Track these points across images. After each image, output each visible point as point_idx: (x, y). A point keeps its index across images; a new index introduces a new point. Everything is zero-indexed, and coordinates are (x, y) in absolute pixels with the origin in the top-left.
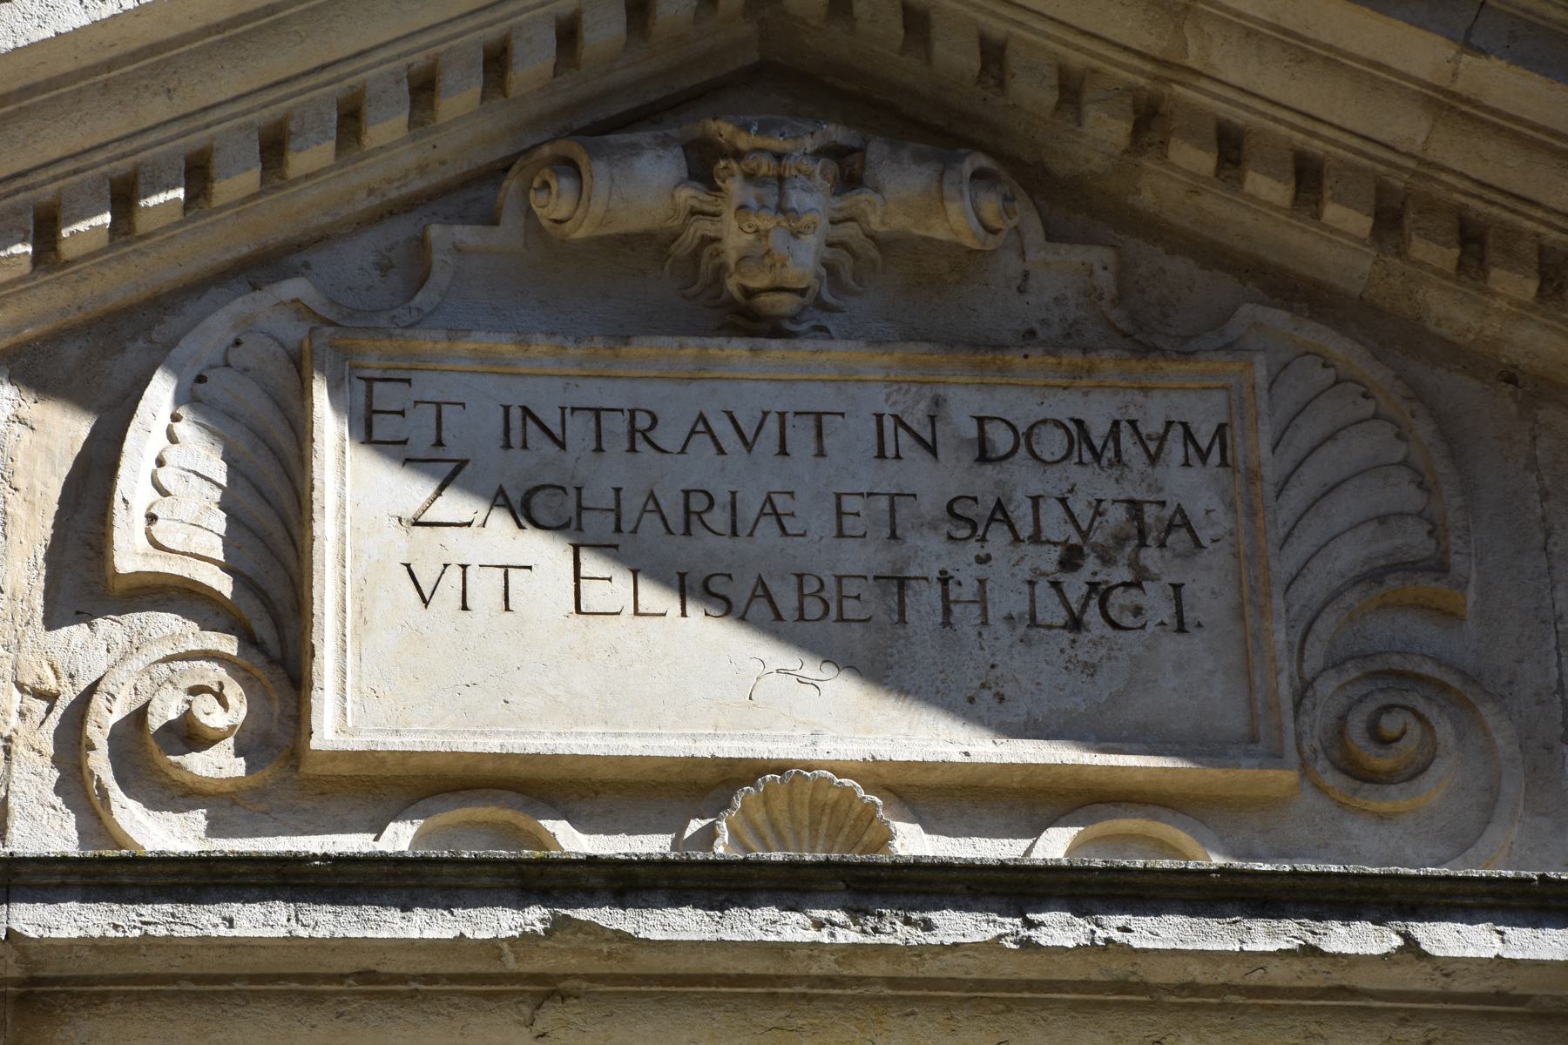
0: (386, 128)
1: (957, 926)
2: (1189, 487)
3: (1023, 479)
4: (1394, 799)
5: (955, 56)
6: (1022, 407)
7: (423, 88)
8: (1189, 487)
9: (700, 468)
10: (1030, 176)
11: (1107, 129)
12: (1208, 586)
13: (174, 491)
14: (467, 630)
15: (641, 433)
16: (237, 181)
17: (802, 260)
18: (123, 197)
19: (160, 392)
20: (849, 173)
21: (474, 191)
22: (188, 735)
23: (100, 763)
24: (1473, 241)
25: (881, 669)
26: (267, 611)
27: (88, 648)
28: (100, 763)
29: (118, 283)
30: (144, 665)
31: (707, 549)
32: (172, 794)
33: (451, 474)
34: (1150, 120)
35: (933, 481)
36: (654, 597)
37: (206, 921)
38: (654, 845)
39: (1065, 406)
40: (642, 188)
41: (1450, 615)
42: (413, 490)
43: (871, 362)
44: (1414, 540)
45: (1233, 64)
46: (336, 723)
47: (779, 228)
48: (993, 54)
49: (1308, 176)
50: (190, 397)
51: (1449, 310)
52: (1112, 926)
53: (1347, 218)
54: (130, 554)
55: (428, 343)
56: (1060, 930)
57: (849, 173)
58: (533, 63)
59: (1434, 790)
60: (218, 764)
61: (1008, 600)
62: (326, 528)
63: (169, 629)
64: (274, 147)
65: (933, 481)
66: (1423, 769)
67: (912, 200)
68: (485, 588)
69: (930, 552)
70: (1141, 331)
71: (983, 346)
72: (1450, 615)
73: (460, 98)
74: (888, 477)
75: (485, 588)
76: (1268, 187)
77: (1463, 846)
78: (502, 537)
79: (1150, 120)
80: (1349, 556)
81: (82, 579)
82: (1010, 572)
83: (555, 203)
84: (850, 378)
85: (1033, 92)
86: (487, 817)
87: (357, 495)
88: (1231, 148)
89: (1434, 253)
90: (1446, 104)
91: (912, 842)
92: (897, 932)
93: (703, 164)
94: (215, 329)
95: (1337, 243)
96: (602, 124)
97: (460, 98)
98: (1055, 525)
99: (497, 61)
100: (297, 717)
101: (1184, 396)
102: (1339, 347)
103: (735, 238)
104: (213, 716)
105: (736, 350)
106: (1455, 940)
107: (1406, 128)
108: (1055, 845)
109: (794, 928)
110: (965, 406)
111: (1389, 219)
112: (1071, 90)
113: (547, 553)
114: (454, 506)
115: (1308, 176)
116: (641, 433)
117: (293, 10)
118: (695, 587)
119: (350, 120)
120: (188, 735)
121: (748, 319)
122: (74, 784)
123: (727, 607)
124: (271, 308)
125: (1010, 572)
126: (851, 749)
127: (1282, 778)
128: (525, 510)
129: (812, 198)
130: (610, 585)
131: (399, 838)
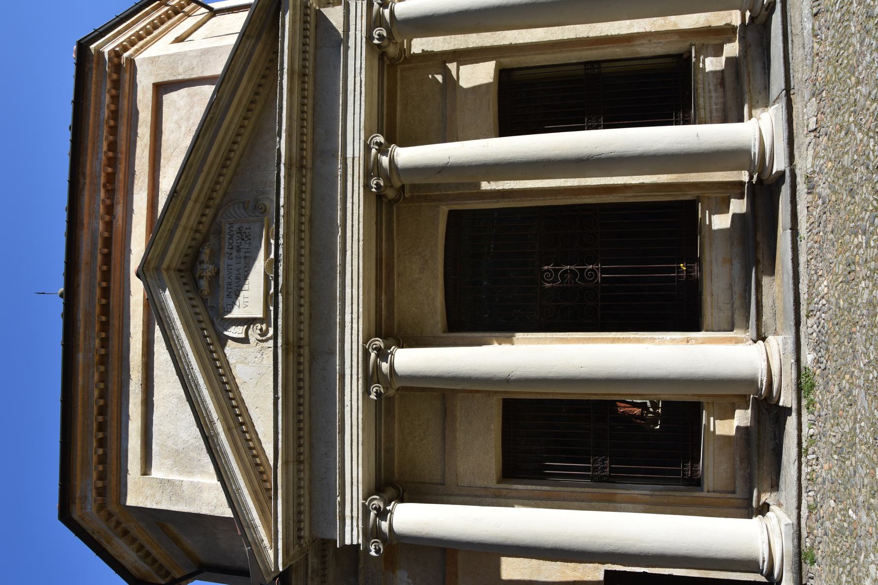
0: (198, 310)
1: (281, 251)
2: (235, 227)
3: (235, 244)
4: (268, 207)
5: (190, 251)
6: (227, 245)
7: (193, 306)
8: (235, 227)
9: (233, 278)
10: (205, 240)
11: (198, 236)
12: (246, 226)
13: (236, 332)
14: (250, 301)
15: (230, 284)
16: (204, 325)
17: (211, 267)
18: (205, 337)
19: (225, 333)
20: (202, 262)
21: (204, 301)
22: (261, 330)
23: (264, 338)
24: (210, 198)
25: (254, 259)
26: (248, 322)
27: (252, 339)
28: (264, 338)
29: (214, 337)
30: (254, 334)
31: (242, 277)
32: (267, 331)
33: (234, 303)
34: (197, 231)
35: (235, 254)
36: (247, 282)
37: (280, 327)
38: (272, 282)
39: (227, 240)
40: (204, 284)
41: (249, 202)
42: (236, 307)
43: (222, 260)
44: (241, 205)
45: (191, 222)
46: (260, 314)
47: (208, 269)
48: (190, 247)
49: (203, 215)
50: (226, 330)
51: (217, 201)
52: (281, 236)
53: (207, 211)
54: (243, 336)
55: (220, 306)
56: (281, 241)
57: (202, 262)
58: (191, 295)
59: (267, 204)
60: (264, 327)
61: (247, 246)
62: (240, 316)
63: (250, 332)
64: (200, 322)
65: (235, 254)
66: (219, 270)
67: (205, 255)
68: (246, 300)
69: (242, 254)
70: (219, 232)
71: (221, 248)
72: (249, 202)
73: (194, 303)
74: (234, 259)
75: (246, 300)
76: (204, 219)
77: (272, 201)
78: (241, 298)
79: (197, 231)
80: (243, 211)
81: (245, 340)
82: (244, 246)
83: (205, 293)
84: (224, 262)
85: (194, 243)
86: (269, 299)
87: (236, 313)
88: (200, 223)
89: (211, 202)
90: (196, 201)
91: (272, 256)
92: (281, 258)
93: (201, 277)
94: (219, 328)
95: (210, 212)
96: (197, 288)
97: (194, 303)
98: (239, 241)
99: (190, 299)
100: (259, 319)
101: (226, 228)
102: (221, 211)
103: (209, 274)
104: (259, 327)
105: (221, 274)
106: (282, 202)
107: (198, 205)
108: (272, 242)
109: (281, 268)
110: (227, 250)
111: (208, 207)
112: (193, 239)
113: (242, 294)
114: (237, 303)
115: (203, 215)
116: (230, 284)
117: (396, 459)
118: (246, 278)
119: (197, 314)
120: (261, 330)
121: (218, 273)
122: (266, 341)
123: (248, 275)
124: (217, 322)
125: (244, 246)
126: (263, 262)
127: (266, 218)
128: (238, 296)
129: (205, 266)
130: (246, 287)
131: (272, 308)
